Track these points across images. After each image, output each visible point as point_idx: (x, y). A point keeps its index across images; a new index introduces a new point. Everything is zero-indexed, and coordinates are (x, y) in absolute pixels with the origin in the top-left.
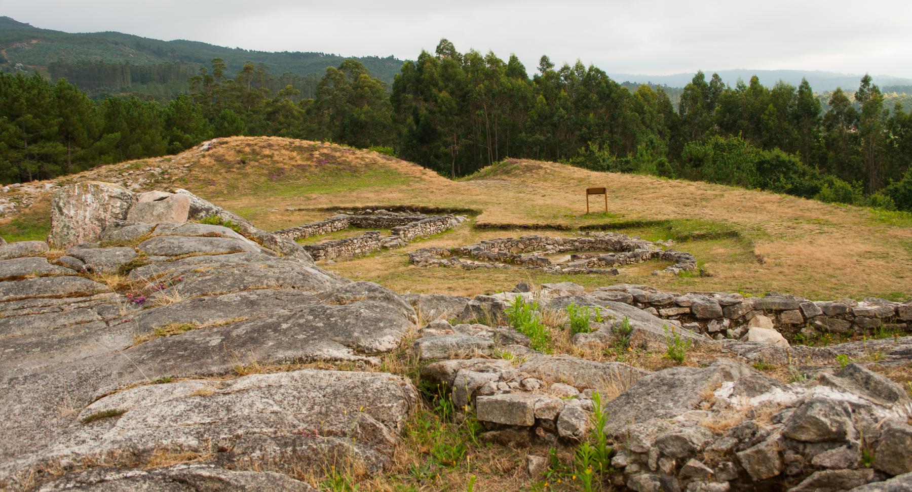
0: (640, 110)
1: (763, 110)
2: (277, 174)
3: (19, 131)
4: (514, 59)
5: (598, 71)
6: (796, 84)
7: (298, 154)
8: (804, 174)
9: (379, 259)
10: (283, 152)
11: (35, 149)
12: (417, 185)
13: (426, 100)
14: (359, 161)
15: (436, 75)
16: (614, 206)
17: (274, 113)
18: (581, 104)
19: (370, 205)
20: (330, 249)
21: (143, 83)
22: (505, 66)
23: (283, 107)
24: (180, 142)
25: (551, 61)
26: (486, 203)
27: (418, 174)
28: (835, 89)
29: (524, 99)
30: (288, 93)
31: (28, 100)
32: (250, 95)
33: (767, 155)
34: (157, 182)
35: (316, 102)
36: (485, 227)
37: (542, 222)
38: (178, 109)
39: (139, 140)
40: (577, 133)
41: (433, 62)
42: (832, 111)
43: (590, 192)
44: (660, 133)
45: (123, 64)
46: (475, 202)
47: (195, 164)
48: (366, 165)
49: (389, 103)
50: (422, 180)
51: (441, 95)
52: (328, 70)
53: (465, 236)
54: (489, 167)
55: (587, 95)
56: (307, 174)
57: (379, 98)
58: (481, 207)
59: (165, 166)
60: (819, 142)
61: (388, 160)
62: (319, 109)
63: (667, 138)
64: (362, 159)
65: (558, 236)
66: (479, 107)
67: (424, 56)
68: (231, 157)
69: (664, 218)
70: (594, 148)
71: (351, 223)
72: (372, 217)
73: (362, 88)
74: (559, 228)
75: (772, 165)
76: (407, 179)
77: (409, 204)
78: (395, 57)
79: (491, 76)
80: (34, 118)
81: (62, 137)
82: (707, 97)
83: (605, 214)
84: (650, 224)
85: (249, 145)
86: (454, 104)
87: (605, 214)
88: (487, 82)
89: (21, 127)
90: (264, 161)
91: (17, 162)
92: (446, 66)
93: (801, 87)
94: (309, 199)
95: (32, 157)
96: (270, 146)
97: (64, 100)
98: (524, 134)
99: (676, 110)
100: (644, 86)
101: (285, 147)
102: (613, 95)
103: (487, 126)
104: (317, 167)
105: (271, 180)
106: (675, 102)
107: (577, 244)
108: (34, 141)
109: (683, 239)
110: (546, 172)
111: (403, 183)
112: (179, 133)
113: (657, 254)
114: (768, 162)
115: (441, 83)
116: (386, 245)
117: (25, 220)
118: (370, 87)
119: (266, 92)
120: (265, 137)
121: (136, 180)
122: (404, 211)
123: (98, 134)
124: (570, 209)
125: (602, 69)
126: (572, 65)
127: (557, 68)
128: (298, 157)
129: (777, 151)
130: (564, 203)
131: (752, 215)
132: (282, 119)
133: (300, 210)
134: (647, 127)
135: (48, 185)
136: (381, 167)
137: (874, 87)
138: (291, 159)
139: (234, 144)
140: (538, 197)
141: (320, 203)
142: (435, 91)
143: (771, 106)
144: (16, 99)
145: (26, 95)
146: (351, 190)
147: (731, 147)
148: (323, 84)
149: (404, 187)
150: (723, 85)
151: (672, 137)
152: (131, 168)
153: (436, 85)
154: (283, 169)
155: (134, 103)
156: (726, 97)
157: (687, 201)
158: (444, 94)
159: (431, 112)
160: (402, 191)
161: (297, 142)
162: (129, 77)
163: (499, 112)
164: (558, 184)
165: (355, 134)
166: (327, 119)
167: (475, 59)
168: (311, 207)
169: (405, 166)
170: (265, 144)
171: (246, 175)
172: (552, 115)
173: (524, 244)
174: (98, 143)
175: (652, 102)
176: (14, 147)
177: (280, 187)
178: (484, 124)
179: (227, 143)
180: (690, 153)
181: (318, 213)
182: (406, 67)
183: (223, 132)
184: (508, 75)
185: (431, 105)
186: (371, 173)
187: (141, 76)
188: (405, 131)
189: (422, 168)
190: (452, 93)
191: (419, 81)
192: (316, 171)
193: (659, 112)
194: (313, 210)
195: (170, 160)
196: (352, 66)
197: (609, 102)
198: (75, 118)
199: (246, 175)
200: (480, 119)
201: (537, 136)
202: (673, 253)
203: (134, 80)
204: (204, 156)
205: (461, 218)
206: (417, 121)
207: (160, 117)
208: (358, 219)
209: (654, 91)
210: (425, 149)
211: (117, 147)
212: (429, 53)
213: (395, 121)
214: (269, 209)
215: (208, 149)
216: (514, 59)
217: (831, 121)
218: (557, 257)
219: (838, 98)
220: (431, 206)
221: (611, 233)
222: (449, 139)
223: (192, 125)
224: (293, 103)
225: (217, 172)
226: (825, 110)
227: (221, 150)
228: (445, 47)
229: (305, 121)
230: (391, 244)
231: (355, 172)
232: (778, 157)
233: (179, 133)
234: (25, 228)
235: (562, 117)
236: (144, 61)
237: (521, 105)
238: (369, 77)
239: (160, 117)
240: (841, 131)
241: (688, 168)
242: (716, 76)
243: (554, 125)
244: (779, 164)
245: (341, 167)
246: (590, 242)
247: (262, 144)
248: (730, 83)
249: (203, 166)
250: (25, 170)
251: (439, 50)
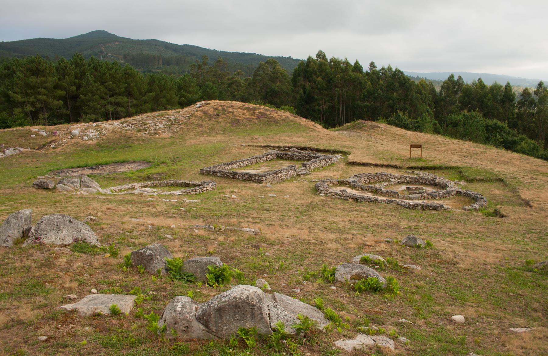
0: (420, 92)
1: (485, 97)
2: (235, 122)
3: (105, 90)
4: (357, 63)
5: (399, 71)
6: (504, 84)
7: (247, 112)
8: (509, 133)
9: (296, 183)
10: (239, 110)
11: (112, 99)
12: (311, 133)
13: (310, 82)
14: (279, 117)
15: (316, 69)
16: (425, 154)
17: (232, 84)
18: (390, 88)
19: (287, 145)
20: (268, 176)
21: (168, 65)
23: (236, 81)
24: (185, 98)
25: (376, 64)
26: (352, 148)
27: (312, 127)
28: (524, 88)
29: (360, 83)
30: (239, 74)
31: (110, 74)
32: (220, 74)
33: (491, 122)
34: (172, 124)
35: (253, 79)
36: (353, 164)
37: (386, 163)
38: (185, 81)
39: (164, 97)
40: (387, 103)
41: (315, 62)
42: (522, 100)
43: (412, 146)
44: (429, 105)
46: (345, 147)
47: (192, 115)
48: (283, 120)
49: (290, 82)
50: (314, 130)
51: (318, 79)
52: (260, 64)
53: (342, 169)
54: (349, 124)
55: (393, 83)
56: (252, 123)
57: (285, 79)
58: (349, 150)
59: (177, 115)
60: (513, 115)
61: (295, 117)
62: (254, 83)
63: (433, 108)
64: (281, 116)
65: (396, 173)
66: (338, 87)
67: (310, 59)
68: (212, 112)
69: (455, 165)
70: (401, 113)
71: (278, 156)
72: (290, 153)
73: (277, 73)
74: (395, 167)
75: (492, 128)
76: (306, 129)
77: (309, 146)
78: (292, 57)
80: (113, 84)
81: (127, 94)
82: (455, 88)
83: (420, 159)
84: (447, 168)
85: (221, 106)
86: (324, 84)
87: (420, 159)
88: (342, 74)
89: (106, 88)
90: (229, 115)
91: (103, 106)
92: (321, 65)
93: (506, 86)
94: (253, 139)
95: (111, 103)
96: (232, 106)
97: (128, 75)
98: (359, 102)
100: (422, 80)
101: (240, 108)
102: (407, 84)
103: (341, 97)
104: (257, 119)
105: (233, 126)
106: (438, 89)
107: (408, 179)
108: (113, 95)
109: (471, 181)
110: (382, 130)
111: (304, 131)
112: (185, 93)
113: (460, 192)
114: (491, 126)
115: (318, 73)
116: (299, 173)
117: (103, 143)
118: (281, 73)
119: (229, 73)
120: (229, 102)
121: (161, 123)
122: (306, 150)
123: (144, 93)
124: (399, 155)
125: (401, 70)
126: (386, 67)
127: (378, 69)
128: (247, 114)
129: (495, 121)
130: (394, 150)
131: (506, 167)
132: (235, 87)
133: (248, 146)
134: (423, 102)
135: (116, 123)
136: (291, 121)
137: (545, 88)
138: (243, 114)
139: (213, 105)
140: (379, 145)
141: (259, 142)
143: (490, 95)
144: (104, 74)
145: (109, 72)
146: (276, 135)
147: (471, 117)
148: (257, 71)
149: (304, 134)
150: (463, 82)
151: (435, 108)
152: (159, 116)
153: (315, 74)
154: (239, 120)
155: (162, 77)
156: (466, 88)
157: (466, 154)
158: (320, 79)
159: (312, 88)
160: (303, 137)
161: (247, 105)
162: (161, 62)
163: (347, 89)
164: (389, 137)
165: (273, 98)
166: (258, 89)
168: (255, 144)
169: (304, 121)
170: (230, 105)
171: (219, 122)
172: (374, 93)
173: (378, 177)
174: (144, 98)
175: (426, 88)
176: (103, 98)
177: (237, 130)
178: (339, 95)
179: (209, 104)
180: (452, 120)
181: (259, 149)
182: (301, 64)
183: (209, 96)
184: (353, 71)
185: (312, 84)
186: (286, 124)
187: (167, 62)
188: (298, 97)
189: (313, 123)
190: (323, 79)
191: (306, 71)
192: (257, 121)
193: (429, 94)
194: (256, 146)
195: (179, 112)
196: (272, 62)
197: (404, 87)
198: (133, 85)
199: (219, 122)
200: (337, 93)
201: (366, 103)
202: (471, 193)
203: (163, 64)
204: (197, 111)
205: (339, 156)
206: (305, 92)
207: (175, 85)
208: (281, 154)
209: (427, 83)
210: (308, 106)
211: (153, 100)
213: (293, 91)
214: (232, 144)
215: (200, 107)
216: (357, 63)
217: (521, 104)
218: (397, 186)
219: (526, 93)
220: (322, 148)
222: (321, 102)
223: (191, 89)
224: (241, 80)
225: (204, 120)
226: (518, 98)
227: (206, 108)
228: (321, 55)
229: (247, 88)
230: (302, 172)
231: (277, 123)
232: (496, 123)
233: (185, 93)
234: (103, 147)
235: (380, 94)
236: (168, 54)
237: (359, 87)
238: (280, 68)
239: (175, 85)
240: (525, 111)
241: (450, 128)
242: (460, 77)
243: (375, 98)
244: (496, 128)
245: (270, 120)
246: (416, 178)
247: (228, 105)
248: (468, 81)
249: (196, 117)
250: (108, 110)
251: (318, 56)
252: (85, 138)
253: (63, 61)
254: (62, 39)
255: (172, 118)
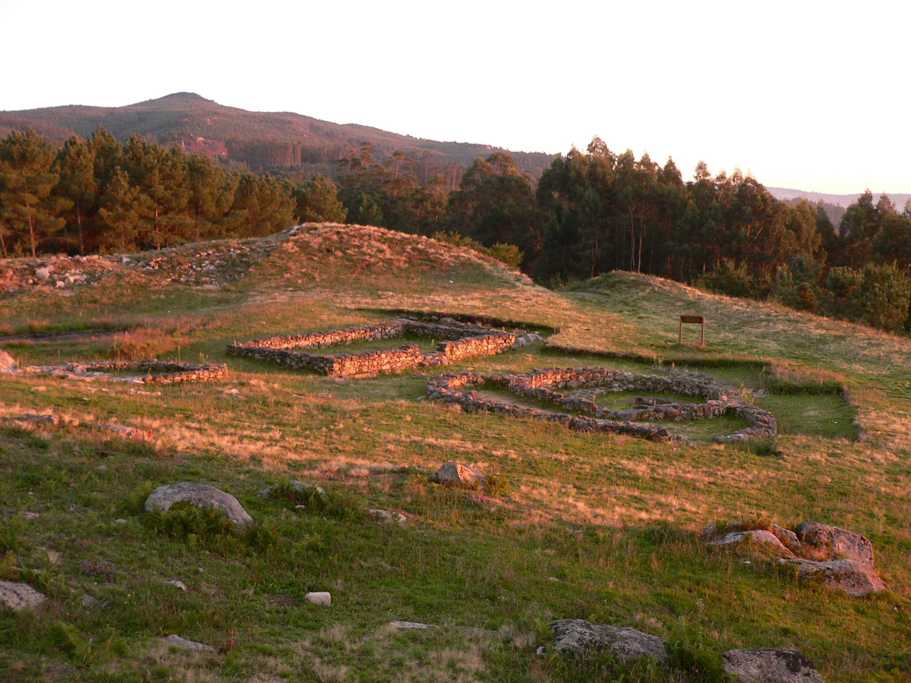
0: (795, 227)
4: (671, 164)
10: (373, 243)
21: (312, 163)
22: (660, 169)
25: (709, 169)
45: (295, 143)
50: (514, 286)
65: (628, 371)
66: (625, 211)
79: (640, 177)
80: (166, 190)
99: (837, 232)
106: (835, 221)
118: (517, 182)
120: (357, 226)
127: (713, 176)
138: (382, 251)
142: (580, 189)
147: (884, 278)
161: (391, 234)
162: (299, 156)
167: (627, 159)
179: (316, 229)
203: (304, 160)
212: (580, 151)
216: (671, 164)
220: (506, 318)
221: (696, 372)
236: (316, 142)
238: (516, 171)
246: (665, 382)
251: (591, 148)
252: (60, 284)
253: (73, 143)
254: (114, 108)
255: (235, 253)
